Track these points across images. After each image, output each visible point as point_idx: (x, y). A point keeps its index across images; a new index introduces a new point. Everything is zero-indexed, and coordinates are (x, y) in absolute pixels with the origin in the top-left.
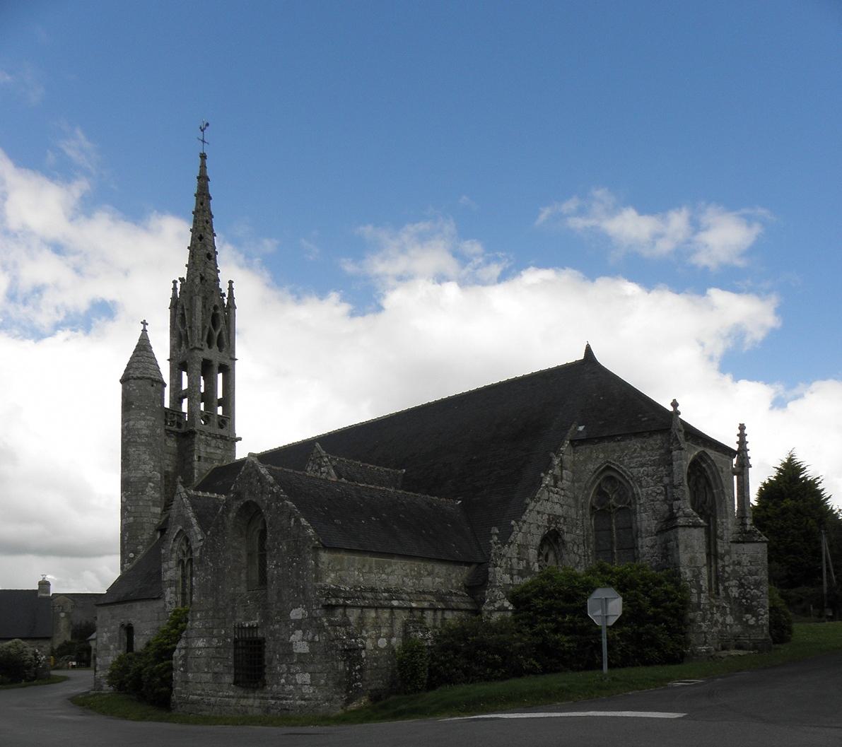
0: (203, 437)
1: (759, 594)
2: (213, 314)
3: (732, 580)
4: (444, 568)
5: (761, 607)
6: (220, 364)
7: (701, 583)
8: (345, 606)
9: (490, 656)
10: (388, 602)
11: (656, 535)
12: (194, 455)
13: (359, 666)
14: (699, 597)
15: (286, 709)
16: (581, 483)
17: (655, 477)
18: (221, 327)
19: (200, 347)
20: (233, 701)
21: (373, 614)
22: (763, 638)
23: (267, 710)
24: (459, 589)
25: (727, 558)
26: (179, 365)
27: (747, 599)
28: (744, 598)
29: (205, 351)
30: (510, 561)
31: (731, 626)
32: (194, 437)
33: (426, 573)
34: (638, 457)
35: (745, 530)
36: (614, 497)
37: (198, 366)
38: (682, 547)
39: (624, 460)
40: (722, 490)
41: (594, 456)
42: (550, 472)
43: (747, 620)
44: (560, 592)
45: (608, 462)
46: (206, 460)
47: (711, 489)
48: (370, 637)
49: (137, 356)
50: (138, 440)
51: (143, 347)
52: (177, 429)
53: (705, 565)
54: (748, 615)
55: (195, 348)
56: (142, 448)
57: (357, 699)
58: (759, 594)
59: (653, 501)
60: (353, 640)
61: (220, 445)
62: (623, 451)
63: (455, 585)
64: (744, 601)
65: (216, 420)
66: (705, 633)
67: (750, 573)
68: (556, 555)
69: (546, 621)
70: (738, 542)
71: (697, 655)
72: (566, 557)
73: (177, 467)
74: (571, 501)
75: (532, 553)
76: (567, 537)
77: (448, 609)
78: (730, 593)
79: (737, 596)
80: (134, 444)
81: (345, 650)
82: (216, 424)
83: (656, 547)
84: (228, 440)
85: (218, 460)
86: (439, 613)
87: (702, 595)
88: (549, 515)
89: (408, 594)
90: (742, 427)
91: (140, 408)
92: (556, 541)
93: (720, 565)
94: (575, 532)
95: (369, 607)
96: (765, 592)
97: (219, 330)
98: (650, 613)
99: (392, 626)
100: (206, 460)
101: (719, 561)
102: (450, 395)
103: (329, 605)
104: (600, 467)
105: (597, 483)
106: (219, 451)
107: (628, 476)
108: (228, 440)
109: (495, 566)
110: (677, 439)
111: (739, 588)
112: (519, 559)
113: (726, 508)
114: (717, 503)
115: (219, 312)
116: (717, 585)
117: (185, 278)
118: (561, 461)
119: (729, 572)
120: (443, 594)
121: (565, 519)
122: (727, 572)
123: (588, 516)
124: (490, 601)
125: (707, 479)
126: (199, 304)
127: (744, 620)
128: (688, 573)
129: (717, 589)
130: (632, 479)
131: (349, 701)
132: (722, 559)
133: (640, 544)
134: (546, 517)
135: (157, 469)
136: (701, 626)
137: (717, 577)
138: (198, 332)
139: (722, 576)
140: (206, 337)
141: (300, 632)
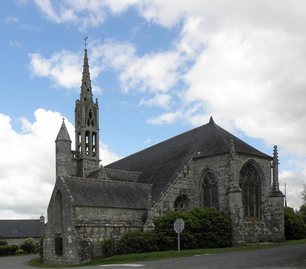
0: (86, 161)
1: (280, 218)
2: (90, 113)
3: (268, 213)
4: (132, 211)
5: (281, 224)
6: (93, 132)
7: (240, 215)
8: (85, 227)
9: (136, 244)
10: (104, 225)
11: (225, 196)
12: (83, 168)
13: (87, 248)
14: (239, 221)
15: (67, 263)
16: (198, 175)
17: (225, 172)
18: (93, 117)
19: (84, 126)
20: (56, 259)
21: (97, 229)
22: (281, 237)
23: (63, 262)
24: (139, 219)
25: (266, 203)
26: (78, 134)
27: (275, 221)
28: (273, 220)
29: (87, 127)
30: (160, 208)
31: (267, 232)
32: (83, 161)
33: (123, 214)
34: (219, 164)
35: (275, 192)
36: (211, 180)
37: (84, 134)
38: (231, 200)
39: (213, 165)
40: (264, 175)
41: (203, 164)
42: (182, 172)
43: (275, 230)
44: (170, 220)
45: (207, 166)
46: (88, 169)
47: (258, 175)
48: (96, 237)
49: (61, 132)
50: (61, 164)
51: (63, 128)
52: (77, 158)
53: (241, 208)
54: (275, 228)
55: (83, 127)
56: (63, 167)
57: (86, 259)
58: (280, 218)
59: (224, 181)
60: (86, 239)
61: (93, 163)
62: (213, 161)
63: (137, 218)
64: (273, 221)
65: (91, 154)
66: (241, 235)
67: (276, 210)
68: (186, 205)
69: (163, 231)
70: (271, 197)
71: (237, 244)
72: (190, 205)
73: (77, 173)
74: (193, 183)
75: (171, 205)
76: (190, 198)
77: (132, 227)
78: (267, 219)
79: (270, 219)
80: (60, 165)
81: (81, 242)
82: (92, 155)
83: (225, 200)
84: (96, 161)
85: (93, 169)
86: (127, 229)
87: (240, 220)
88: (180, 189)
89: (114, 221)
90: (275, 147)
91: (62, 151)
92: (185, 199)
93: (262, 207)
94: (195, 195)
95: (95, 226)
96: (282, 218)
97: (92, 119)
98: (211, 228)
99: (105, 233)
100: (88, 169)
101: (262, 205)
102: (172, 137)
103: (77, 226)
104: (205, 168)
105: (204, 176)
106: (93, 166)
107: (215, 172)
108: (96, 161)
109: (150, 210)
110: (232, 156)
111: (271, 216)
112: (164, 207)
113: (266, 182)
114: (261, 181)
115: (92, 111)
116: (261, 215)
117: (80, 99)
118: (188, 167)
119: (267, 209)
120: (131, 221)
121: (189, 190)
122: (266, 210)
123: (201, 189)
124: (147, 224)
125: (256, 170)
126: (84, 109)
127: (273, 229)
128: (234, 211)
129: (261, 217)
130: (216, 173)
131: (82, 260)
132: (263, 204)
133: (219, 199)
134: (179, 190)
135: (68, 174)
136: (239, 233)
137: (261, 212)
138: (84, 120)
139: (263, 211)
140: (87, 122)
141: (70, 236)
